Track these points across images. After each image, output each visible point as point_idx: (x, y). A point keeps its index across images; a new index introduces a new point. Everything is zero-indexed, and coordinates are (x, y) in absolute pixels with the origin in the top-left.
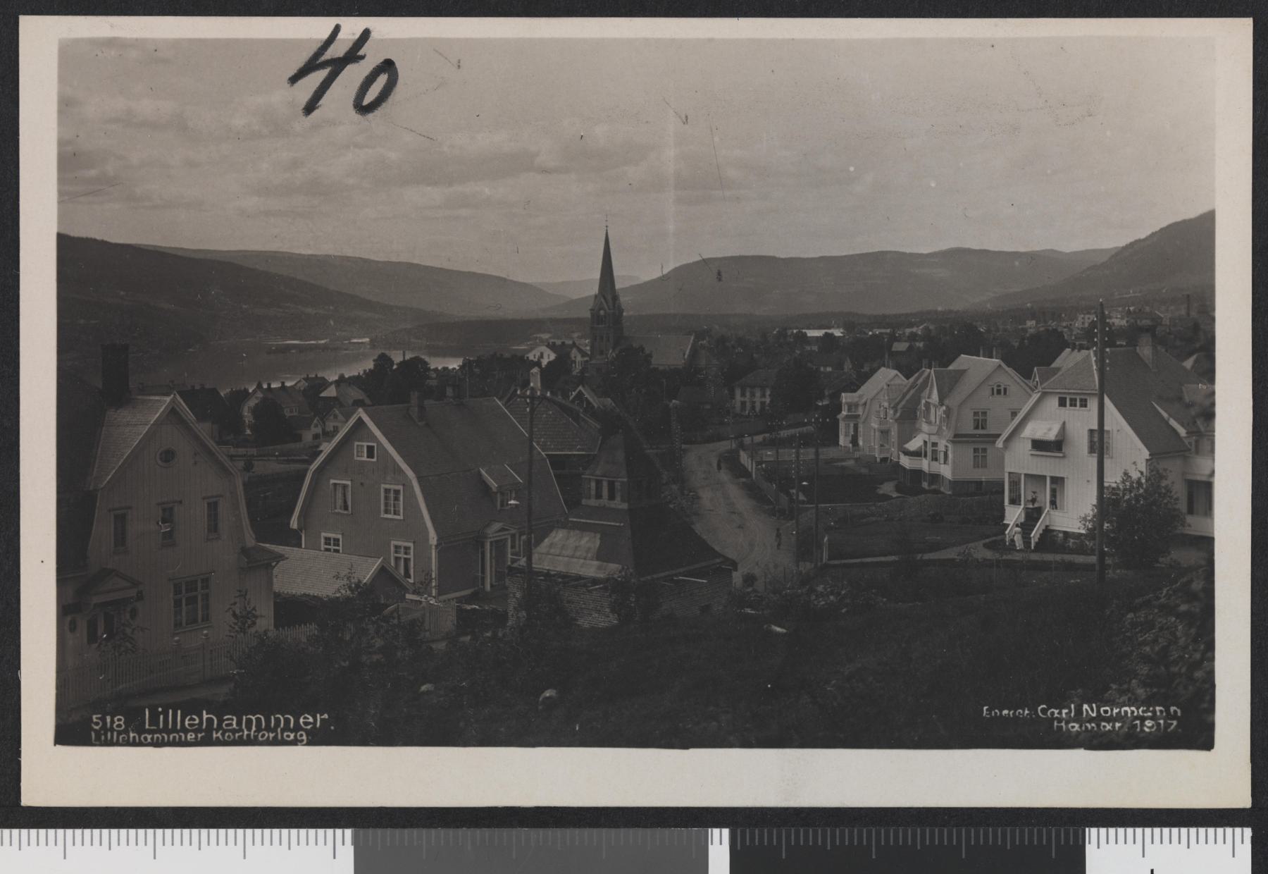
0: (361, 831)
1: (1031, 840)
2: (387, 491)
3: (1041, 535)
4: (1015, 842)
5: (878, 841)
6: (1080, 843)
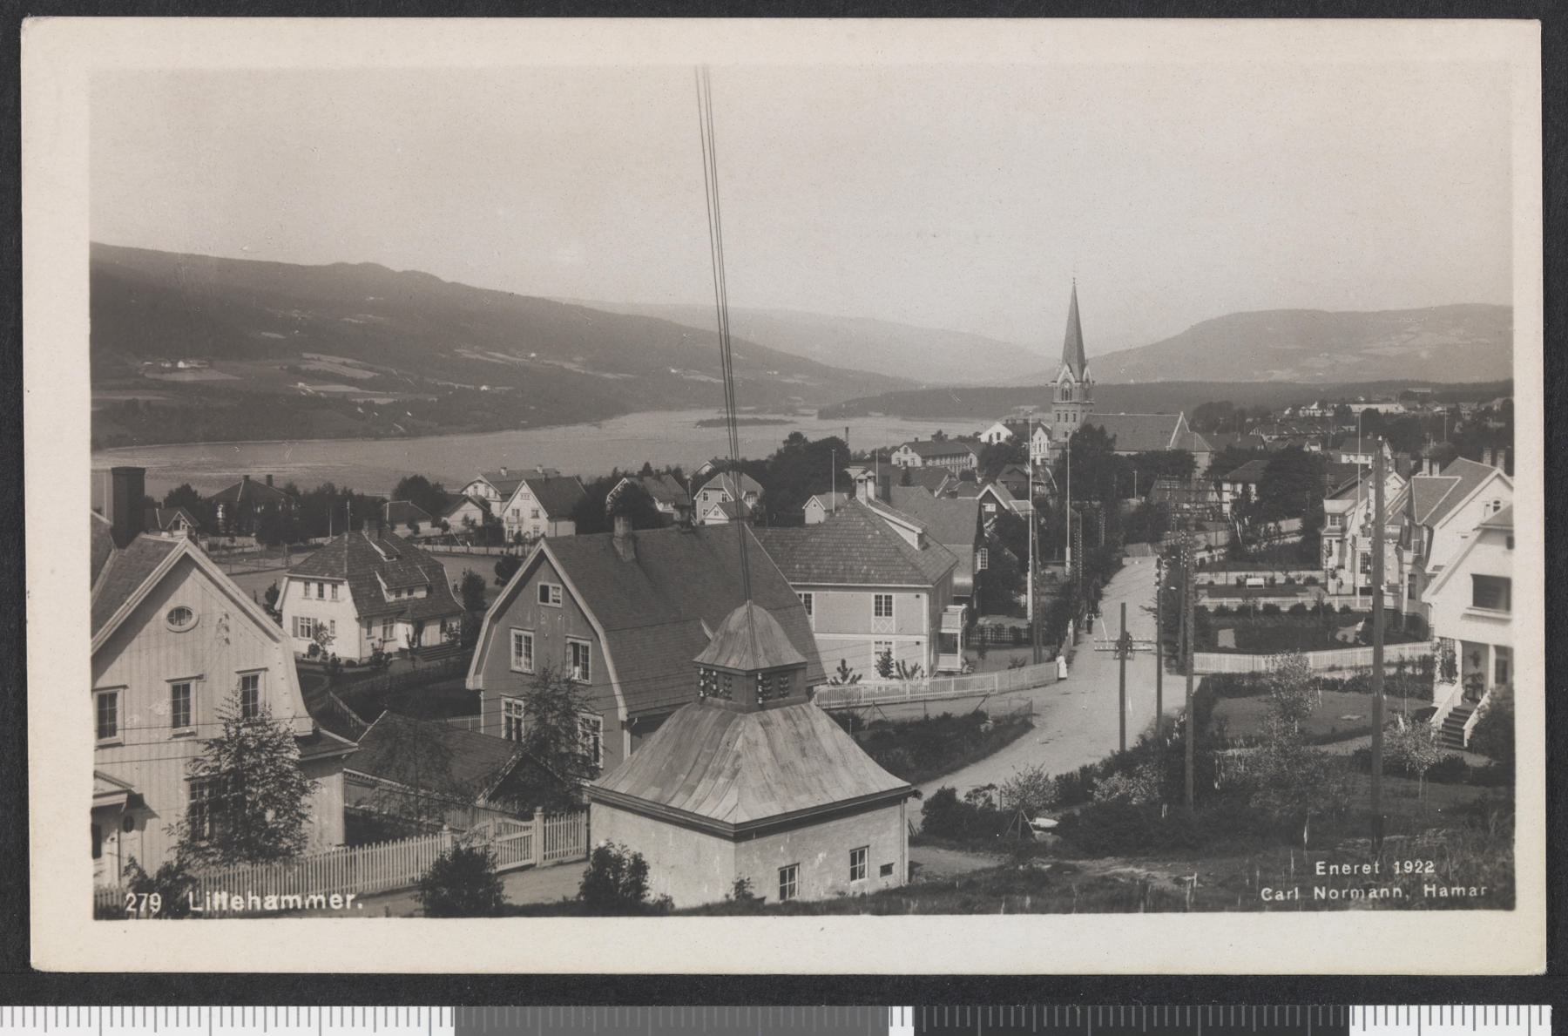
0: (463, 1009)
1: (963, 1021)
2: (519, 638)
3: (946, 717)
4: (1043, 1023)
5: (1315, 1019)
6: (1342, 1024)
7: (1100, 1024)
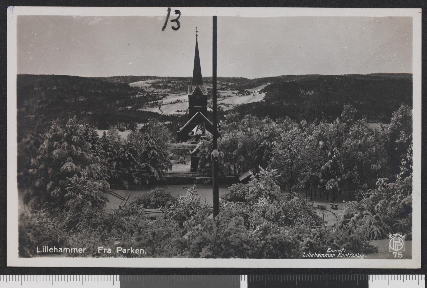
0: (122, 276)
6: (367, 280)
7: (254, 280)
